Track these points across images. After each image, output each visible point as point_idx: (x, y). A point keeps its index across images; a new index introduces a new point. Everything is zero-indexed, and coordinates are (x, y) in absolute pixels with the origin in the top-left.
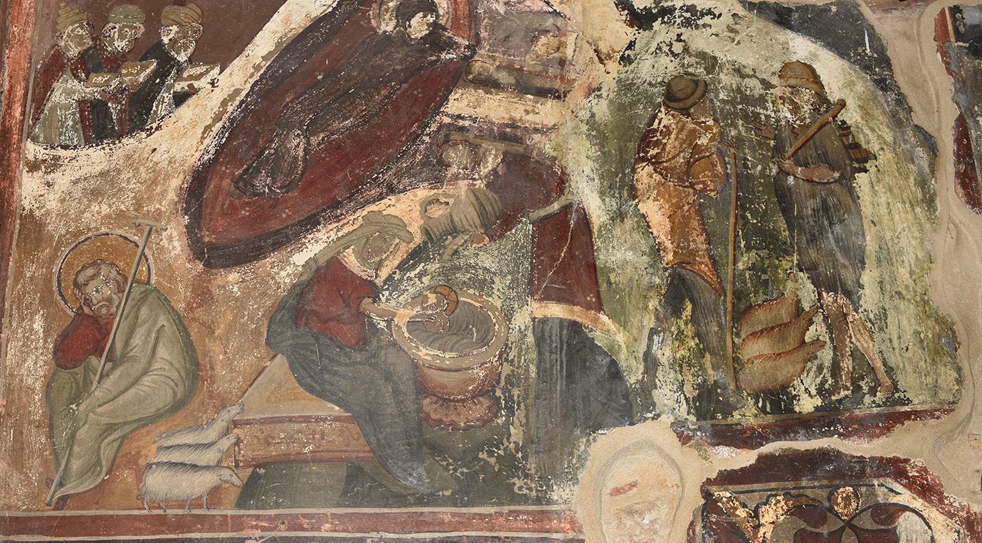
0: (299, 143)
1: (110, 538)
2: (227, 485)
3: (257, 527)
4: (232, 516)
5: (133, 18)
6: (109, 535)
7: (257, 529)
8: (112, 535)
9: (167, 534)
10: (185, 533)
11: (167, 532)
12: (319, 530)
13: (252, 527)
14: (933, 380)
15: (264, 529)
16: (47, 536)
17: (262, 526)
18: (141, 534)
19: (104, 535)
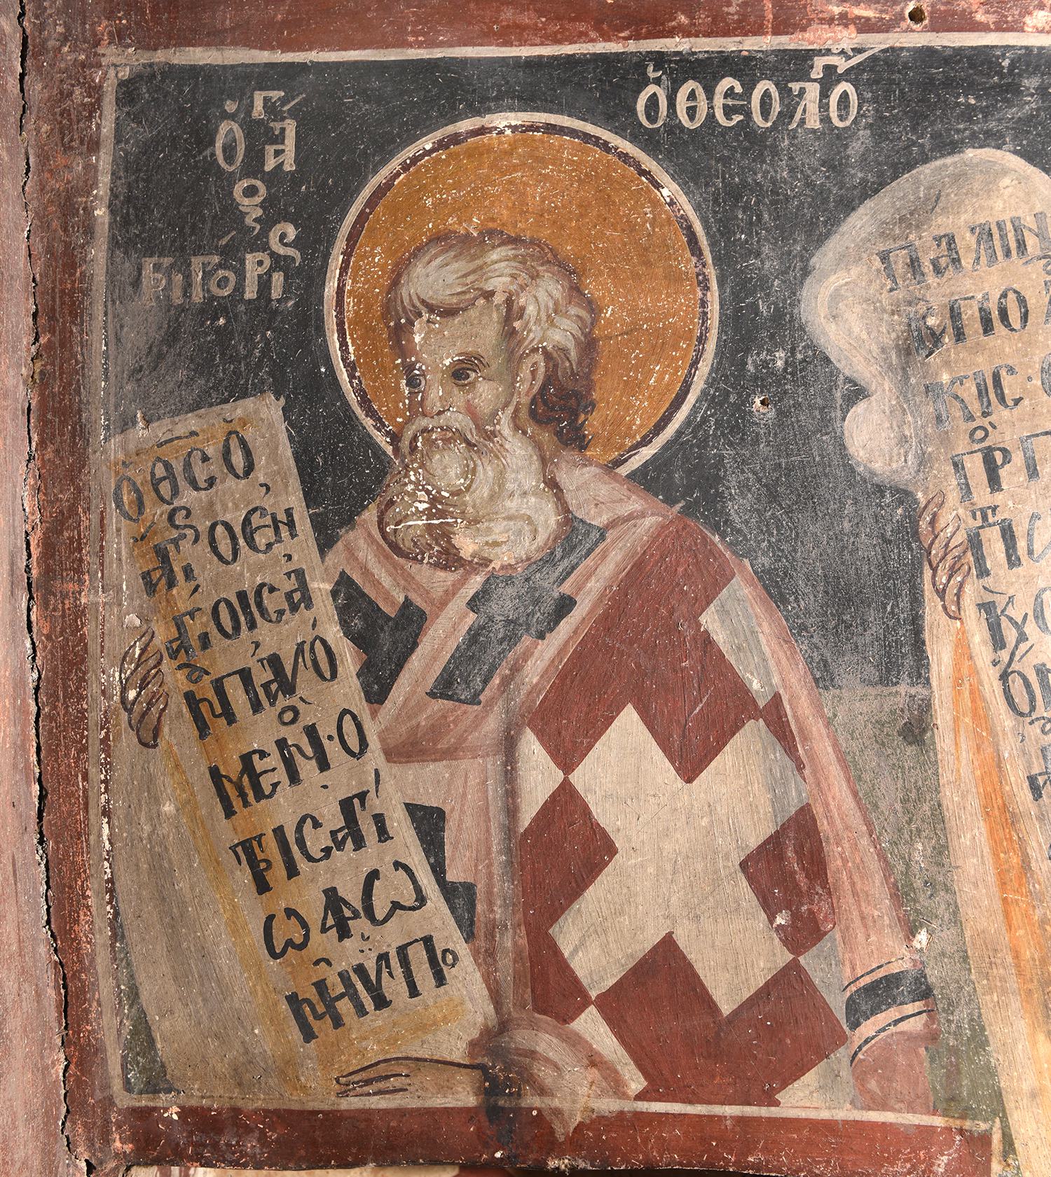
0: (121, 1022)
1: (438, 53)
2: (166, 865)
3: (844, 20)
4: (758, 31)
5: (561, 408)
6: (432, 44)
7: (846, 26)
8: (441, 45)
9: (592, 41)
10: (645, 38)
11: (593, 34)
12: (1017, 27)
13: (830, 21)
14: (413, 239)
15: (865, 26)
16: (262, 49)
17: (859, 18)
18: (523, 42)
19: (420, 45)
